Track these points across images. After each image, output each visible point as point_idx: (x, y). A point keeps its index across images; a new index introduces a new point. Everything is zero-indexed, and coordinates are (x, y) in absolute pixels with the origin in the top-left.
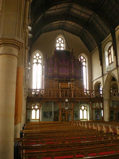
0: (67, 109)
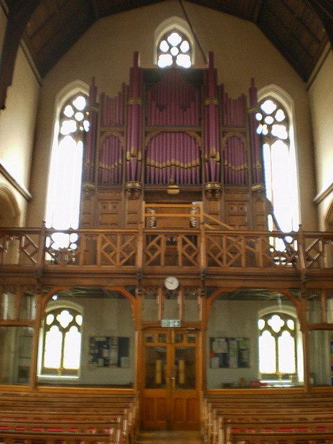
0: (171, 326)
